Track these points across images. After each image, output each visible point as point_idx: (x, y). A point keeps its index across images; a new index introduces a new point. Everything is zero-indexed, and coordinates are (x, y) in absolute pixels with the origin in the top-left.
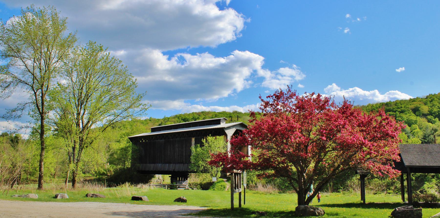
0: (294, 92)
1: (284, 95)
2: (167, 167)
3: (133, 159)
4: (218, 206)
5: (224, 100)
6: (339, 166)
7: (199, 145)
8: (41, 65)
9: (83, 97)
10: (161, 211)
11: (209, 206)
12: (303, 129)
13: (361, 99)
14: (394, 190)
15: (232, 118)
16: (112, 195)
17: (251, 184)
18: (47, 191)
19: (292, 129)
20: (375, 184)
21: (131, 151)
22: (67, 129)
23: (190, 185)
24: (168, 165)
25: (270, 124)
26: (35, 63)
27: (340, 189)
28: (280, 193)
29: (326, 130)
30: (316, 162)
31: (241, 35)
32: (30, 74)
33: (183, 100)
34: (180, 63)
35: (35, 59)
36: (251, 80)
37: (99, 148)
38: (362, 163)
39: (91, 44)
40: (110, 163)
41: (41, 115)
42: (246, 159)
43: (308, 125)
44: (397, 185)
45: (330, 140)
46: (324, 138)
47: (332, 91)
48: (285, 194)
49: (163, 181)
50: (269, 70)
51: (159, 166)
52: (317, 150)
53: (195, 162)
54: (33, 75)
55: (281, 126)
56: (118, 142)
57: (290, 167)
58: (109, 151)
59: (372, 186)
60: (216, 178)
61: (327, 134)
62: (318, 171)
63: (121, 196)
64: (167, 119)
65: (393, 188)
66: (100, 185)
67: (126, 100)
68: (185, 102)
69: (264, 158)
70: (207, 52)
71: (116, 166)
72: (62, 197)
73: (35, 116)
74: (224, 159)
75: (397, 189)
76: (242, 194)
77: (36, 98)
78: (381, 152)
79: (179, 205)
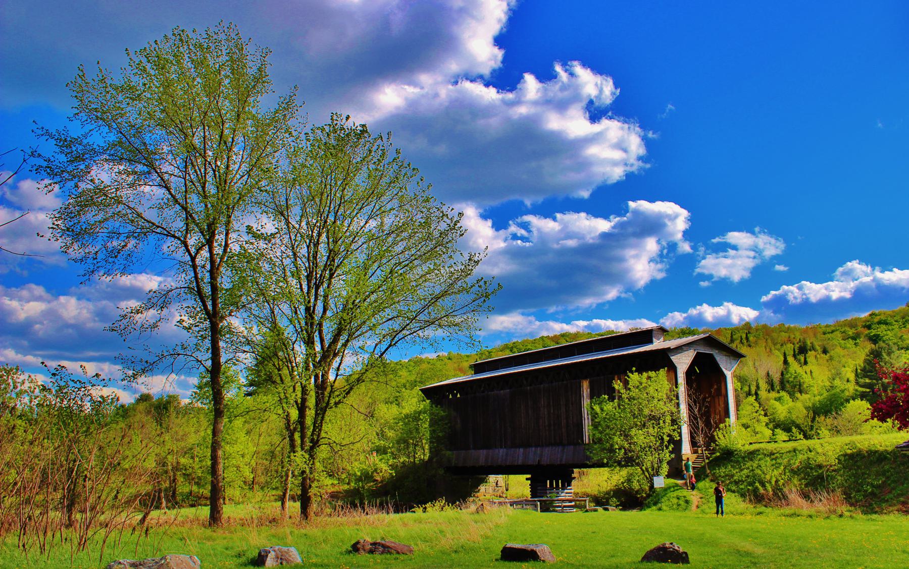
2: (519, 455)
3: (435, 440)
9: (321, 264)
24: (522, 450)
33: (520, 311)
51: (500, 454)
54: (185, 208)
64: (487, 353)
68: (523, 314)
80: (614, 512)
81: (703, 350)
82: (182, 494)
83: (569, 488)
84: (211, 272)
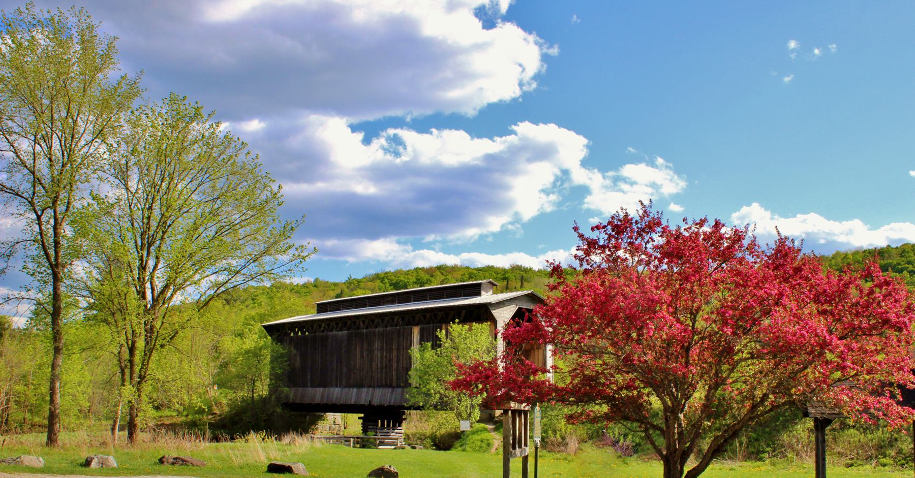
0: (656, 217)
2: (352, 395)
3: (274, 376)
6: (765, 397)
7: (429, 344)
8: (53, 150)
9: (153, 228)
13: (822, 241)
14: (896, 458)
15: (509, 283)
16: (221, 459)
17: (552, 439)
19: (651, 305)
20: (850, 444)
21: (269, 356)
23: (407, 437)
24: (355, 390)
26: (37, 145)
27: (764, 452)
30: (709, 387)
33: (394, 238)
35: (39, 137)
36: (556, 193)
37: (194, 350)
38: (822, 389)
39: (173, 101)
40: (219, 385)
41: (53, 270)
42: (540, 377)
44: (904, 447)
49: (345, 428)
50: (598, 171)
51: (336, 393)
53: (420, 385)
54: (33, 173)
55: (625, 298)
56: (239, 335)
57: (646, 398)
58: (218, 358)
59: (842, 448)
61: (738, 320)
62: (711, 409)
64: (355, 282)
65: (893, 454)
66: (193, 438)
68: (399, 242)
69: (584, 375)
71: (235, 392)
72: (102, 463)
74: (487, 377)
75: (903, 456)
76: (531, 461)
77: (40, 229)
80: (421, 450)
81: (530, 306)
82: (14, 421)
83: (399, 428)
84: (55, 228)
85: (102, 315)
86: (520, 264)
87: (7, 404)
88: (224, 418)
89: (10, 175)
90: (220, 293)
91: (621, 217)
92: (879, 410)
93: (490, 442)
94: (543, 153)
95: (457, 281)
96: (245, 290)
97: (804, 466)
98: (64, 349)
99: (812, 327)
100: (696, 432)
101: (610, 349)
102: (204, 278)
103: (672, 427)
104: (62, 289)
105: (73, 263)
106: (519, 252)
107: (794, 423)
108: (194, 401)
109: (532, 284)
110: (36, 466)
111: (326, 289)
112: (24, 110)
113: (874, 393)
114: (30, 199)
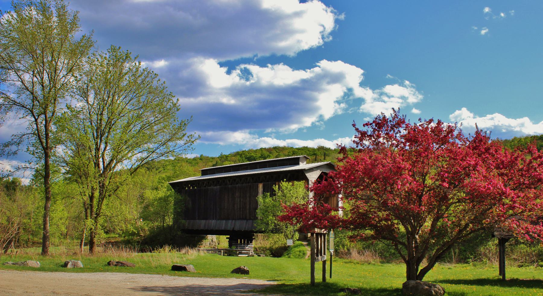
1: (389, 122)
2: (223, 224)
3: (177, 215)
4: (292, 279)
5: (305, 131)
6: (467, 225)
7: (269, 194)
8: (44, 80)
9: (103, 126)
10: (212, 286)
11: (280, 280)
12: (416, 172)
13: (504, 131)
15: (317, 157)
16: (145, 263)
17: (342, 250)
18: (54, 258)
20: (521, 253)
21: (173, 201)
22: (82, 170)
23: (256, 250)
24: (224, 221)
25: (367, 164)
27: (469, 258)
28: (382, 262)
29: (449, 173)
30: (434, 220)
31: (331, 38)
32: (28, 93)
33: (248, 131)
34: (243, 78)
36: (344, 103)
37: (128, 197)
38: (501, 221)
39: (113, 50)
43: (423, 166)
45: (454, 187)
46: (446, 185)
47: (461, 118)
48: (390, 265)
49: (218, 244)
50: (370, 88)
51: (213, 223)
52: (436, 202)
53: (263, 218)
54: (32, 93)
55: (384, 166)
57: (396, 226)
58: (143, 202)
60: (292, 240)
63: (157, 264)
64: (225, 157)
66: (128, 250)
67: (165, 130)
68: (250, 133)
69: (359, 212)
70: (282, 63)
71: (153, 223)
72: (74, 265)
73: (37, 153)
77: (37, 127)
78: (529, 206)
79: (238, 278)
81: (327, 171)
82: (23, 240)
83: (250, 244)
85: (75, 178)
86: (323, 146)
87: (18, 230)
88: (146, 238)
89: (19, 95)
90: (144, 164)
91: (381, 118)
92: (535, 233)
93: (305, 252)
94: (337, 78)
95: (286, 156)
96: (159, 162)
97: (493, 266)
98: (52, 197)
99: (494, 183)
100: (426, 246)
101: (375, 197)
102: (134, 155)
103: (411, 244)
104: (50, 162)
105: (56, 147)
106: (321, 138)
107: (487, 241)
108: (129, 228)
109: (330, 157)
110: (35, 267)
111: (207, 161)
112: (27, 57)
113: (532, 223)
114: (31, 109)
